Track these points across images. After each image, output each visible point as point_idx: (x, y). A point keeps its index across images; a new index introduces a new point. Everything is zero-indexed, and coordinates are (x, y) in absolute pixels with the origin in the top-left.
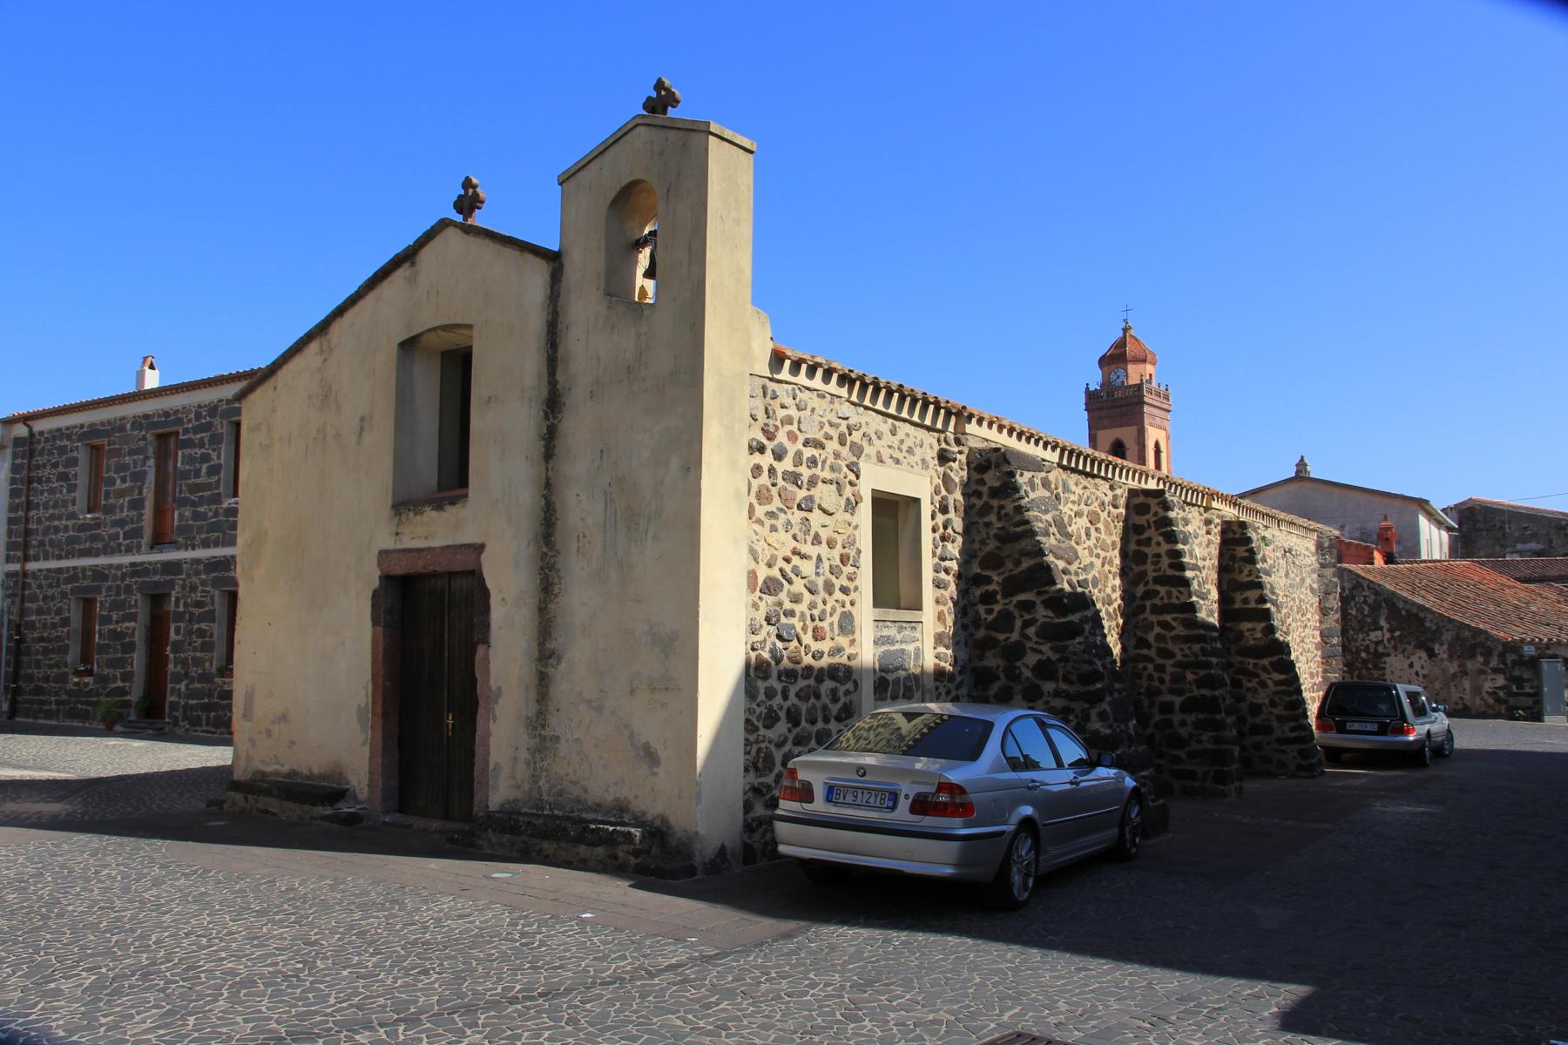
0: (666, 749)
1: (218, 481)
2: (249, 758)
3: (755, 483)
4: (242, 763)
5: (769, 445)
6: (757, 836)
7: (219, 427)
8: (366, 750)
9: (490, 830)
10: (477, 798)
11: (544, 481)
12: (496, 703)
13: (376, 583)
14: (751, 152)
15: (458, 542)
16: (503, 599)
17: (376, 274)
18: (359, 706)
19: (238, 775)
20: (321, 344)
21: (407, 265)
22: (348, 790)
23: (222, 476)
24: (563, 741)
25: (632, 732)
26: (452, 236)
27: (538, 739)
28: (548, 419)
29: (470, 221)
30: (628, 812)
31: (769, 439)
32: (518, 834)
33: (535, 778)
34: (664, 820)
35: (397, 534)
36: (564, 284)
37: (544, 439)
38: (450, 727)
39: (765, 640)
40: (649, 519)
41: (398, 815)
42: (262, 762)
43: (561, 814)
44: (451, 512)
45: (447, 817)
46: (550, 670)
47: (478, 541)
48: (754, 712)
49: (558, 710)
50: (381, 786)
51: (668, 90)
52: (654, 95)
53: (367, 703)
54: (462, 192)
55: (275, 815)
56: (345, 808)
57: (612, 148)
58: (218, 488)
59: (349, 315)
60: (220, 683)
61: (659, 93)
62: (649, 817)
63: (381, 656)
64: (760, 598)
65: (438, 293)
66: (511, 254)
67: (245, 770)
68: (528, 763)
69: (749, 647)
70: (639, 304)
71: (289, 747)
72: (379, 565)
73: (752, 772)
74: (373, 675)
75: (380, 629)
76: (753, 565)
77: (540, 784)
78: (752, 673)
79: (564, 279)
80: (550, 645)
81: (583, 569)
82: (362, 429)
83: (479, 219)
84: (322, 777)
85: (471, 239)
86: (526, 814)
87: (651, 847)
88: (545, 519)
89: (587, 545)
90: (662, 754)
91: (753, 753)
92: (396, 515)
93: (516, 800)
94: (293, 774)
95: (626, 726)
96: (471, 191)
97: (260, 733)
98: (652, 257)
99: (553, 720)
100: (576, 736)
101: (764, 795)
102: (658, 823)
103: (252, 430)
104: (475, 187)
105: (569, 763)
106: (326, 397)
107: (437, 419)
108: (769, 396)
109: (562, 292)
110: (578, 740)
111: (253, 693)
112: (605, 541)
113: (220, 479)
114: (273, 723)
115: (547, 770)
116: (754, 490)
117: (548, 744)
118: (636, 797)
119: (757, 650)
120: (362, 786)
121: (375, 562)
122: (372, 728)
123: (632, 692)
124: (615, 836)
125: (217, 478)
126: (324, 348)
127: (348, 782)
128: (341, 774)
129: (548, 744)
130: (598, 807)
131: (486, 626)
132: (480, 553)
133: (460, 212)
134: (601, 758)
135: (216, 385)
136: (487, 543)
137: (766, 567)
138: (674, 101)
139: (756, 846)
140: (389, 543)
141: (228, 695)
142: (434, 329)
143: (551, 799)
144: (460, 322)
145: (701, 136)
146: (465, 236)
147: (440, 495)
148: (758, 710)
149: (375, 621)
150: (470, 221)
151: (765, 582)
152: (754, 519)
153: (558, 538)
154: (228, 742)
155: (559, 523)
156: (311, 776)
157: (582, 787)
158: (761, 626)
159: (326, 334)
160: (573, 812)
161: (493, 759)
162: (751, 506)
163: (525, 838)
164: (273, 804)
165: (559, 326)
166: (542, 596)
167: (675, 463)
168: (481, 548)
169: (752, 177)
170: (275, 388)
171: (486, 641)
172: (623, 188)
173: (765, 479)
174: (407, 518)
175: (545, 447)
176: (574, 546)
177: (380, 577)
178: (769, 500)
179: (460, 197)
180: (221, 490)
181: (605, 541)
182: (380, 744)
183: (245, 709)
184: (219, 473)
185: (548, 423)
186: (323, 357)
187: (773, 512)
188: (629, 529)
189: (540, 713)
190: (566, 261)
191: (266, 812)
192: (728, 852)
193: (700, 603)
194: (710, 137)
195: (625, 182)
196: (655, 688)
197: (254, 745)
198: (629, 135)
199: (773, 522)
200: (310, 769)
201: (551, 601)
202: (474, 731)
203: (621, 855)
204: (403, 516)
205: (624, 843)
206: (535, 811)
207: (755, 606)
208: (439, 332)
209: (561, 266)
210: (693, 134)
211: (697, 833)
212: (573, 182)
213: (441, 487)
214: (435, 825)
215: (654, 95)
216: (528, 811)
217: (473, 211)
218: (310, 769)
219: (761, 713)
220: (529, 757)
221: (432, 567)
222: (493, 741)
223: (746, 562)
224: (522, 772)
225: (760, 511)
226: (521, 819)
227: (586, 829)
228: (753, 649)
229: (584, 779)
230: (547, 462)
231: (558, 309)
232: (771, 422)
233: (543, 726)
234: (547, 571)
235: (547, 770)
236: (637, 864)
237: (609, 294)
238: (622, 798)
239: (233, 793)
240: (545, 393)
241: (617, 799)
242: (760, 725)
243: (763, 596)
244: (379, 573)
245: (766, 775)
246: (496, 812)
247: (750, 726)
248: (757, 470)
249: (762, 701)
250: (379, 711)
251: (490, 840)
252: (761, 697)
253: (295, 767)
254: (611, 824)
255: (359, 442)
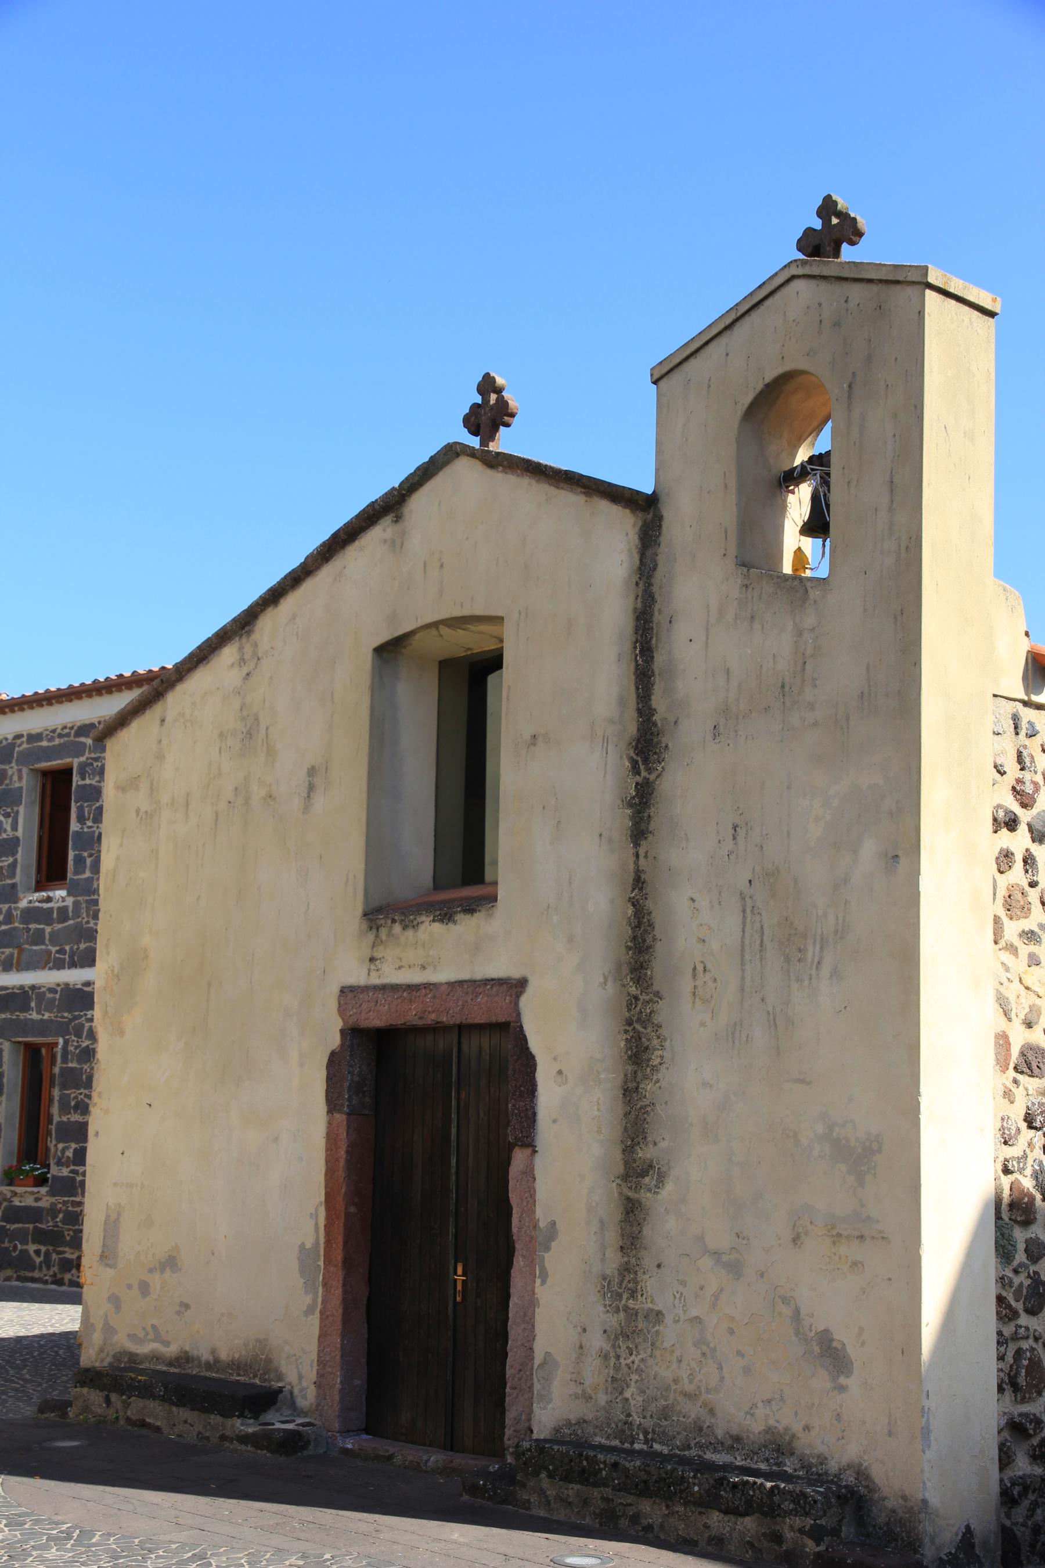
0: (863, 1344)
1: (14, 865)
2: (109, 1329)
3: (1003, 881)
4: (97, 1338)
5: (1025, 816)
6: (1020, 1513)
7: (15, 778)
8: (314, 1323)
9: (543, 1475)
10: (510, 1415)
11: (630, 878)
12: (548, 1249)
13: (335, 1041)
14: (991, 314)
15: (478, 976)
16: (560, 1072)
17: (335, 536)
18: (302, 1245)
19: (89, 1357)
20: (241, 649)
21: (387, 521)
22: (280, 1390)
23: (19, 856)
24: (668, 1320)
25: (797, 1312)
26: (464, 469)
27: (622, 1315)
28: (639, 773)
29: (493, 447)
30: (792, 1454)
31: (1024, 806)
32: (595, 1485)
33: (617, 1384)
34: (862, 1474)
35: (372, 960)
36: (663, 549)
37: (630, 805)
38: (459, 1287)
39: (1025, 1156)
40: (824, 941)
41: (365, 1437)
42: (132, 1337)
43: (666, 1451)
44: (466, 926)
45: (451, 1444)
46: (645, 1196)
47: (515, 973)
48: (1011, 1283)
49: (659, 1266)
50: (338, 1386)
51: (843, 216)
52: (817, 224)
53: (317, 1243)
54: (478, 399)
55: (158, 1429)
56: (278, 1422)
57: (747, 318)
58: (13, 875)
59: (289, 603)
60: (9, 1195)
61: (826, 222)
62: (833, 1466)
63: (342, 1163)
64: (1015, 1081)
65: (442, 566)
66: (570, 499)
67: (101, 1350)
68: (606, 1357)
69: (1000, 1167)
70: (795, 577)
71: (179, 1313)
72: (342, 1011)
73: (1008, 1394)
74: (327, 1195)
75: (340, 1118)
76: (1002, 1024)
77: (627, 1394)
78: (1005, 1216)
79: (663, 539)
80: (645, 1153)
81: (703, 1024)
82: (311, 788)
83: (505, 442)
84: (237, 1365)
85: (500, 478)
86: (602, 1448)
87: (840, 1521)
88: (634, 938)
89: (710, 984)
90: (853, 1352)
91: (1010, 1358)
92: (371, 928)
93: (582, 1422)
94: (184, 1358)
95: (785, 1300)
96: (493, 397)
97: (129, 1287)
98: (815, 499)
99: (650, 1283)
100: (694, 1312)
101: (1030, 1436)
102: (849, 1478)
103: (122, 788)
104: (499, 391)
105: (680, 1361)
106: (249, 735)
107: (434, 768)
108: (1023, 733)
109: (661, 559)
110: (697, 1320)
111: (117, 1221)
112: (743, 979)
113: (16, 861)
114: (151, 1271)
115: (639, 1371)
116: (1002, 892)
117: (641, 1324)
118: (807, 1428)
119: (1012, 1172)
120: (304, 1384)
121: (333, 1005)
122: (325, 1285)
123: (796, 1240)
124: (776, 1499)
125: (11, 859)
126: (247, 656)
127: (280, 1377)
128: (269, 1361)
129: (641, 1324)
130: (736, 1442)
131: (530, 1118)
132: (518, 995)
133: (475, 433)
134: (739, 1353)
135: (13, 711)
136: (530, 978)
137: (1022, 1028)
138: (851, 233)
139: (1019, 1531)
140: (358, 975)
141: (75, 1218)
142: (435, 625)
143: (648, 1423)
144: (479, 612)
145: (911, 291)
146: (490, 472)
147: (432, 898)
148: (1017, 1280)
149: (332, 1104)
150: (493, 447)
151: (1022, 1054)
152: (1002, 944)
153: (657, 970)
154: (75, 1299)
155: (658, 946)
156: (215, 1364)
157: (705, 1404)
158: (1018, 1130)
159: (249, 633)
160: (689, 1448)
161: (541, 1346)
162: (997, 920)
163: (607, 1491)
164: (155, 1412)
165: (656, 617)
166: (629, 1068)
167: (870, 848)
168: (520, 985)
169: (992, 356)
170: (163, 721)
171: (529, 1142)
172: (767, 385)
173: (1017, 874)
174: (390, 934)
175: (632, 818)
176: (686, 986)
177: (342, 1031)
178: (1026, 910)
179: (475, 407)
180: (17, 879)
181: (743, 979)
182: (338, 1313)
183: (104, 1245)
184: (14, 853)
185: (638, 779)
186: (245, 670)
187: (1032, 932)
188: (787, 960)
189: (626, 1269)
190: (667, 511)
191: (143, 1424)
192: (977, 1541)
193: (922, 1089)
194: (928, 292)
195: (770, 376)
196: (839, 1235)
197: (118, 1308)
198: (778, 296)
199: (1032, 948)
200: (213, 1352)
201: (646, 1077)
202: (506, 1297)
203: (789, 1535)
204: (383, 932)
205: (794, 1513)
206: (616, 1443)
207: (1008, 1095)
208: (444, 630)
209: (659, 519)
210: (898, 287)
211: (925, 1501)
212: (677, 377)
213: (438, 885)
214: (435, 1458)
215: (817, 224)
216: (603, 1441)
217: (497, 430)
218: (213, 1352)
219: (1021, 1285)
220: (607, 1347)
221: (433, 1016)
222: (542, 1318)
223: (992, 1020)
224: (593, 1373)
225: (1012, 930)
226: (601, 1457)
227: (721, 1482)
228: (1006, 1171)
229: (708, 1391)
230: (637, 844)
231: (655, 589)
232: (1027, 776)
233: (633, 1294)
234: (638, 1027)
235: (639, 1371)
236: (819, 1555)
237: (744, 564)
238: (780, 1427)
239: (85, 1390)
240: (632, 729)
241: (768, 1430)
242: (1019, 1306)
243: (1020, 1077)
244: (339, 1024)
245: (1031, 1400)
246: (545, 1441)
247: (1005, 1311)
248: (1005, 858)
249: (1021, 1265)
250: (338, 1255)
251: (542, 1492)
252: (1020, 1257)
253: (187, 1348)
254: (768, 1476)
255: (307, 807)
